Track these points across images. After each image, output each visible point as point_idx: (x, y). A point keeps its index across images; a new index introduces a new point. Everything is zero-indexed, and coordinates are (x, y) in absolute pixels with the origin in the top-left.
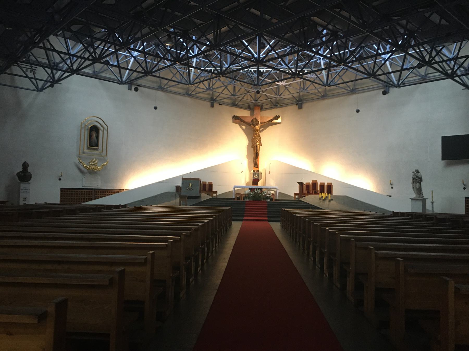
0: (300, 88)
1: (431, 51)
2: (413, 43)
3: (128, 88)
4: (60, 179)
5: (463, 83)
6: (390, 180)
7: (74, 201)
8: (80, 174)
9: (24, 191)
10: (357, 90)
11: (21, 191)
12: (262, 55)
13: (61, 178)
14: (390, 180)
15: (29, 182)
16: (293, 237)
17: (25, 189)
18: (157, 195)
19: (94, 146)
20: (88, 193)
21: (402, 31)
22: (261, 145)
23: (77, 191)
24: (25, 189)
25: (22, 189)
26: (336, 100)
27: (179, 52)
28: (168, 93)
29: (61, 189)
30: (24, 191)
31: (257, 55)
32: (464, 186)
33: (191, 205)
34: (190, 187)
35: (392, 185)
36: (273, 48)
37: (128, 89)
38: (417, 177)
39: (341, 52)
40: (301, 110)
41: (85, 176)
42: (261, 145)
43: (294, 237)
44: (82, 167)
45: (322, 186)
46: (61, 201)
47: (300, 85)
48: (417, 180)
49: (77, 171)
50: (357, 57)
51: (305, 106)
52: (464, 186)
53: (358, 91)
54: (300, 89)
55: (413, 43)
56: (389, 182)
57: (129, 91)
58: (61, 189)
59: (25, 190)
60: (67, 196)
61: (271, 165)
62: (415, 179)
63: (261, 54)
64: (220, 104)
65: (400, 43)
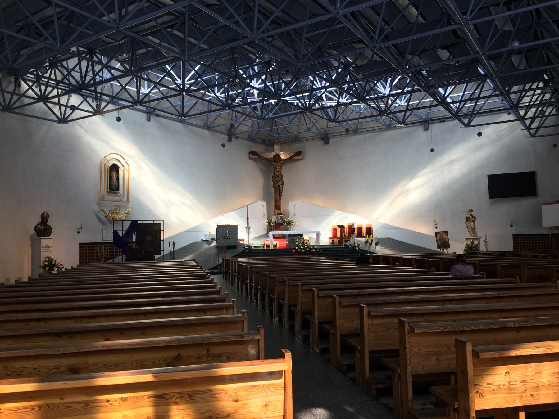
0: (232, 119)
1: (365, 86)
2: (348, 79)
3: (146, 118)
4: (79, 232)
5: (49, 100)
6: (435, 220)
7: (533, 248)
8: (99, 225)
9: (46, 249)
10: (393, 126)
11: (43, 249)
12: (188, 80)
13: (80, 230)
14: (435, 220)
15: (50, 237)
16: (247, 293)
17: (46, 246)
18: (185, 246)
19: (115, 189)
20: (109, 248)
21: (336, 65)
22: (283, 184)
23: (89, 247)
24: (46, 246)
25: (43, 246)
26: (368, 135)
27: (352, 92)
28: (186, 125)
29: (80, 244)
30: (46, 249)
31: (180, 80)
32: (510, 224)
33: (232, 256)
34: (228, 235)
35: (436, 224)
36: (199, 75)
37: (147, 120)
38: (471, 215)
39: (275, 83)
40: (327, 145)
41: (105, 227)
42: (284, 185)
43: (248, 293)
44: (101, 216)
45: (360, 229)
46: (514, 248)
47: (232, 116)
48: (471, 219)
49: (95, 220)
50: (291, 88)
51: (331, 141)
52: (510, 224)
53: (393, 127)
54: (232, 120)
55: (348, 79)
56: (434, 222)
57: (148, 121)
58: (80, 244)
59: (46, 248)
60: (518, 243)
61: (296, 207)
62: (469, 218)
63: (187, 79)
64: (236, 138)
65: (333, 78)
